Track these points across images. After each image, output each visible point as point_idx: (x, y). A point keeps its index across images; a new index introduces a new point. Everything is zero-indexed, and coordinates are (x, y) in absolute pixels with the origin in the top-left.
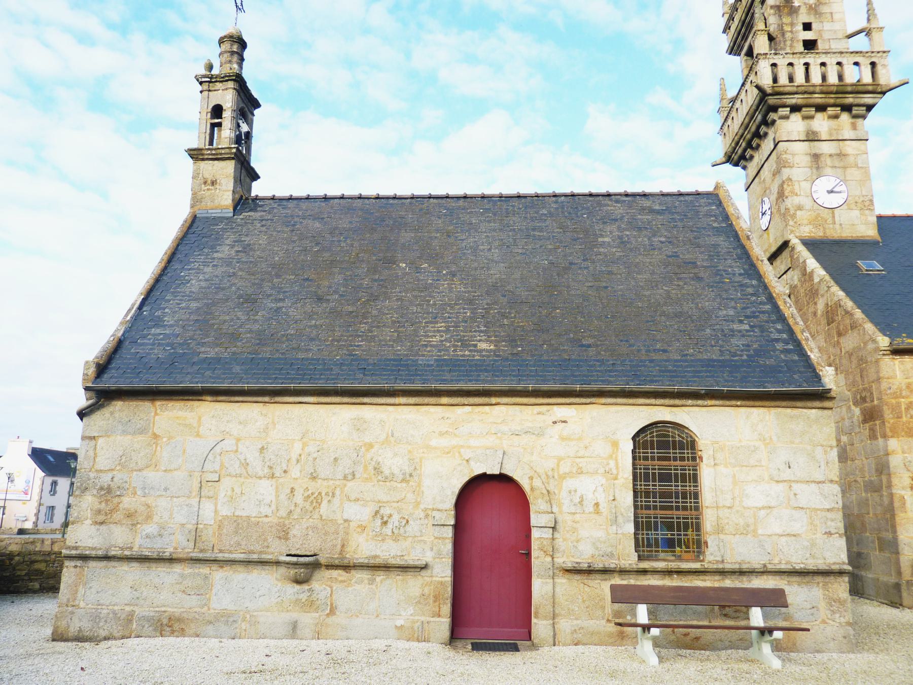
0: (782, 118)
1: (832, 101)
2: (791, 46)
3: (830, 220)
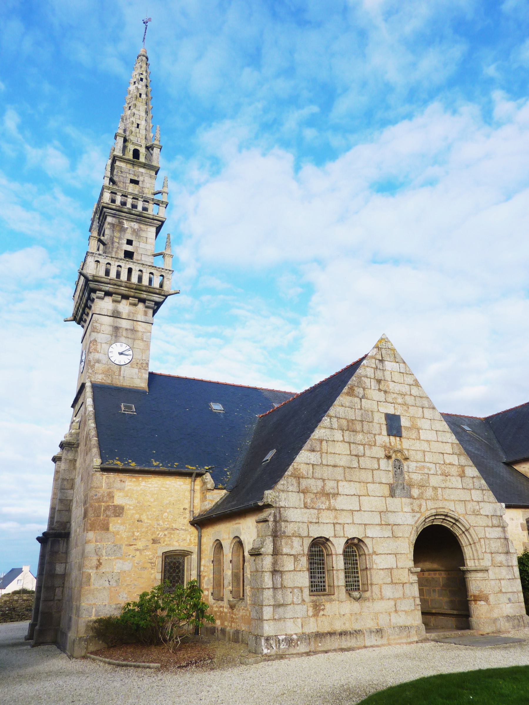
0: (98, 298)
1: (132, 294)
2: (116, 252)
3: (117, 373)
